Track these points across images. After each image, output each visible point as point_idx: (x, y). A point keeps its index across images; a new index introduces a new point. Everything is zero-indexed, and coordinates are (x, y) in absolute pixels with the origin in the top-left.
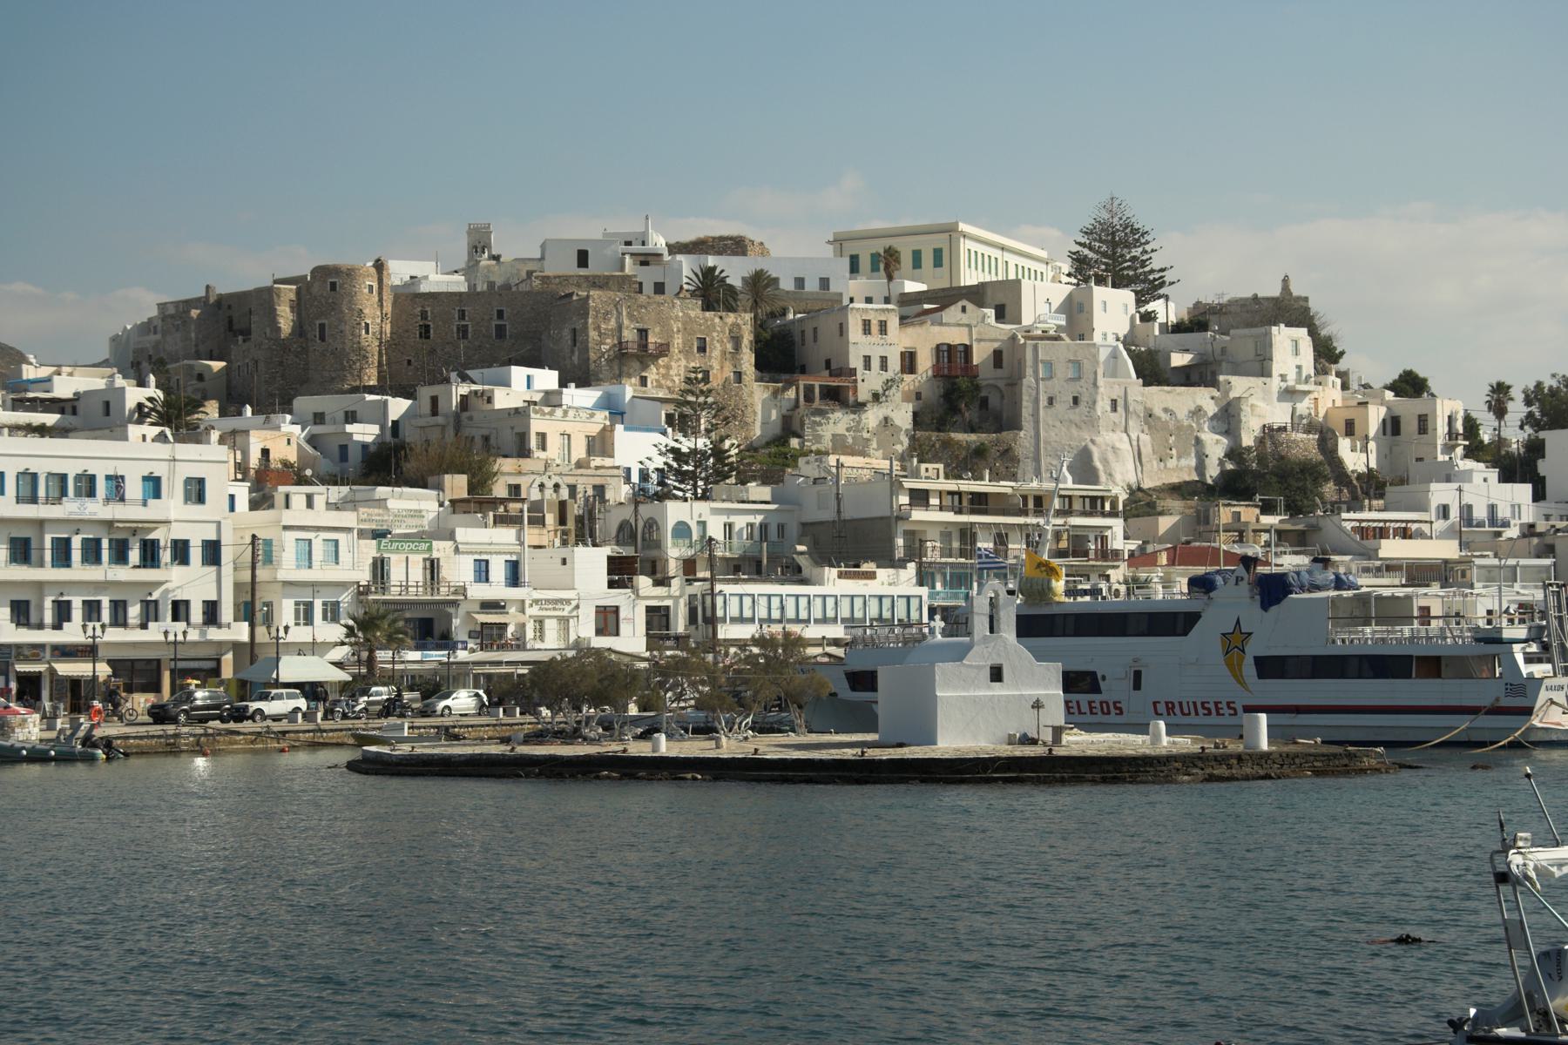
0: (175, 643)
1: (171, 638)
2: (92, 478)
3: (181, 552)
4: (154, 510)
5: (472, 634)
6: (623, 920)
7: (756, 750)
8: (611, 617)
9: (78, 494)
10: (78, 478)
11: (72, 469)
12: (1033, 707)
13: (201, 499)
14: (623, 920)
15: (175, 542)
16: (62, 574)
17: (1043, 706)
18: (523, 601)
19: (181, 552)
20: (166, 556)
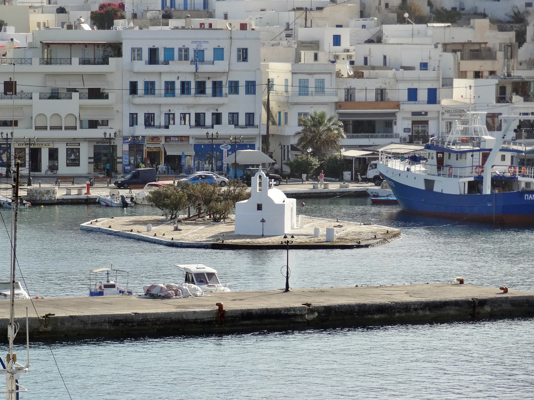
0: (7, 139)
1: (108, 136)
2: (187, 50)
3: (234, 87)
4: (220, 66)
5: (406, 130)
6: (73, 395)
7: (172, 238)
8: (251, 117)
9: (180, 59)
10: (180, 50)
11: (176, 45)
12: (261, 222)
13: (245, 59)
14: (73, 395)
15: (231, 82)
16: (170, 100)
17: (265, 222)
18: (439, 111)
19: (234, 87)
20: (225, 90)
